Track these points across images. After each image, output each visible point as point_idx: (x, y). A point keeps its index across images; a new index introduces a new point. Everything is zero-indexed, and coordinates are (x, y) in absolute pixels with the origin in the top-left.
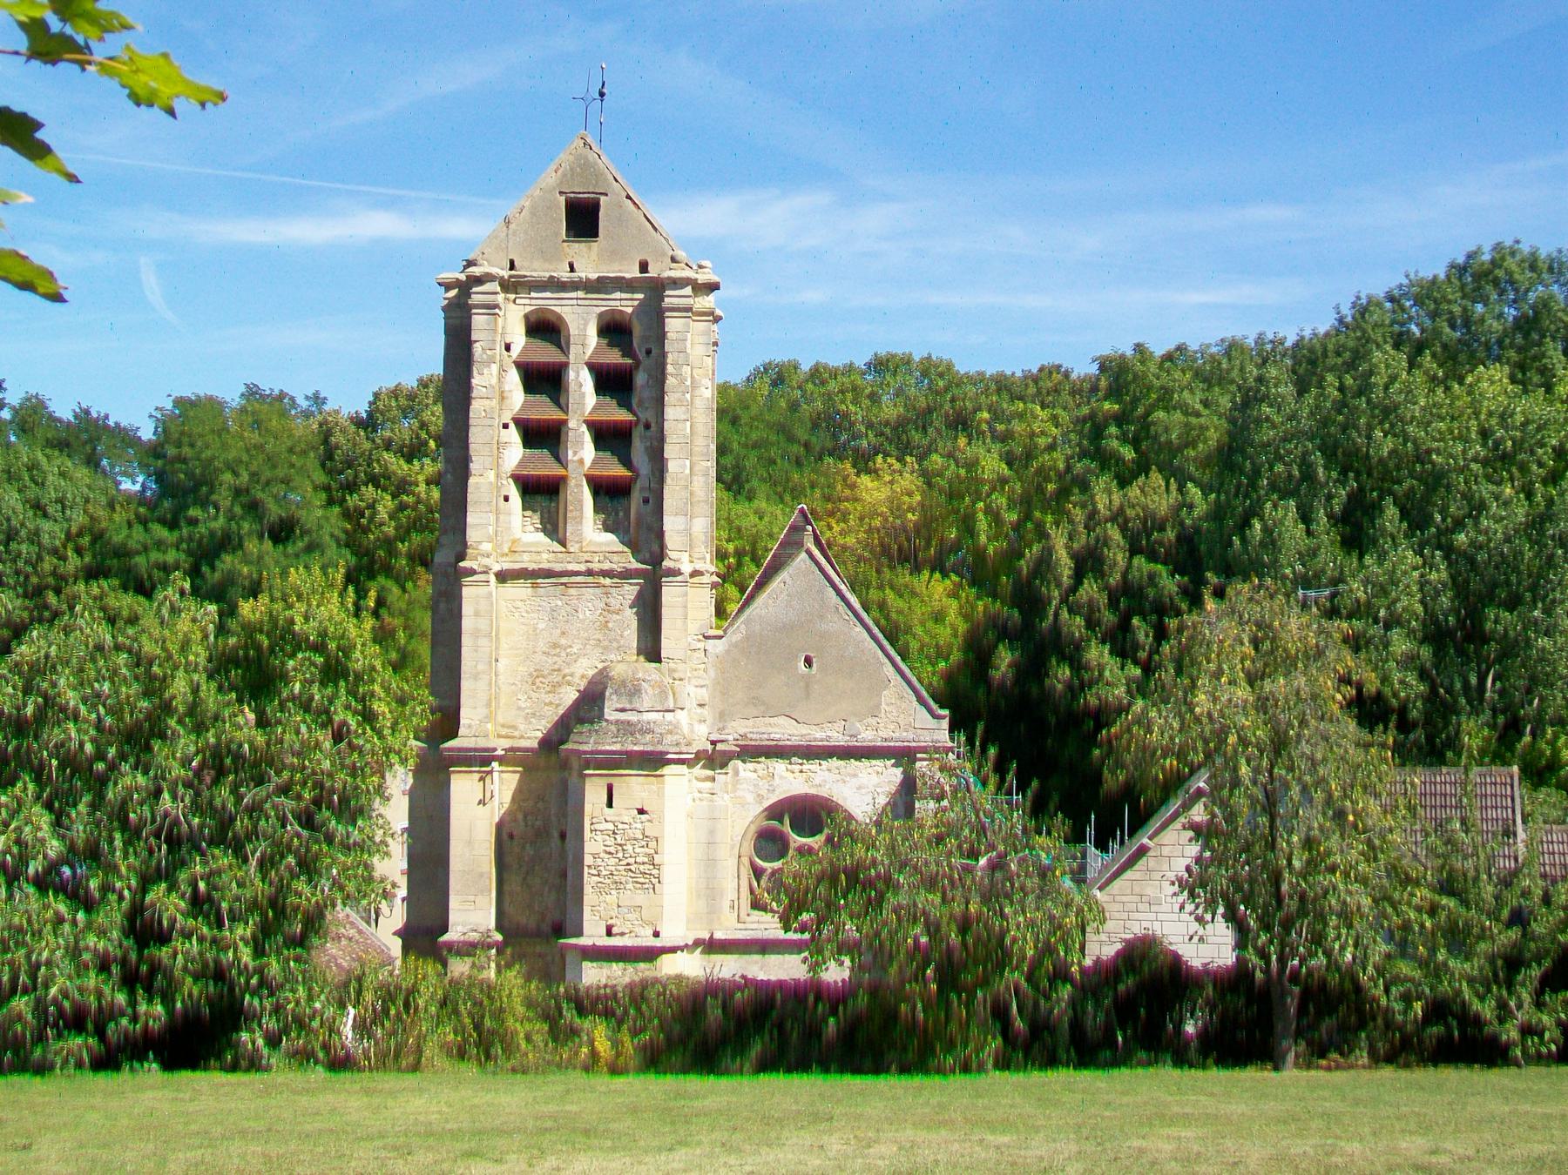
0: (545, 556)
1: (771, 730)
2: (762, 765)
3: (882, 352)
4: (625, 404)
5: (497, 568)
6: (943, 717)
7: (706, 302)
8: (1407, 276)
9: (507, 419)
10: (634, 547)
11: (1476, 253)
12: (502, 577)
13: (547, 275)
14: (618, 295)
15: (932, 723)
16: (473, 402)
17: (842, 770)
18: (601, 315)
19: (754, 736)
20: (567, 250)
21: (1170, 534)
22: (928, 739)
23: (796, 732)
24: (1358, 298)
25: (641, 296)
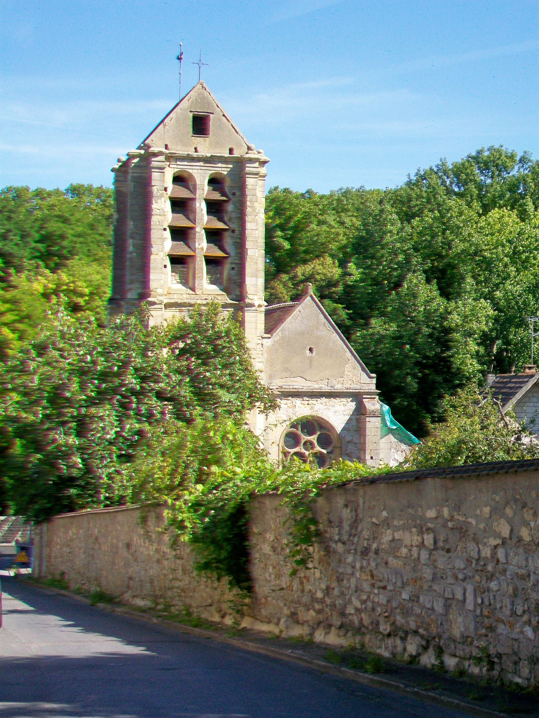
0: (185, 296)
1: (293, 384)
2: (290, 401)
3: (75, 183)
4: (221, 219)
5: (166, 301)
6: (373, 378)
7: (263, 170)
8: (441, 160)
9: (166, 226)
10: (226, 290)
11: (482, 151)
12: (168, 306)
13: (186, 153)
14: (220, 165)
15: (368, 380)
16: (153, 217)
17: (328, 404)
18: (211, 175)
19: (286, 387)
20: (194, 141)
21: (340, 288)
22: (367, 388)
23: (305, 385)
24: (419, 170)
25: (231, 166)
